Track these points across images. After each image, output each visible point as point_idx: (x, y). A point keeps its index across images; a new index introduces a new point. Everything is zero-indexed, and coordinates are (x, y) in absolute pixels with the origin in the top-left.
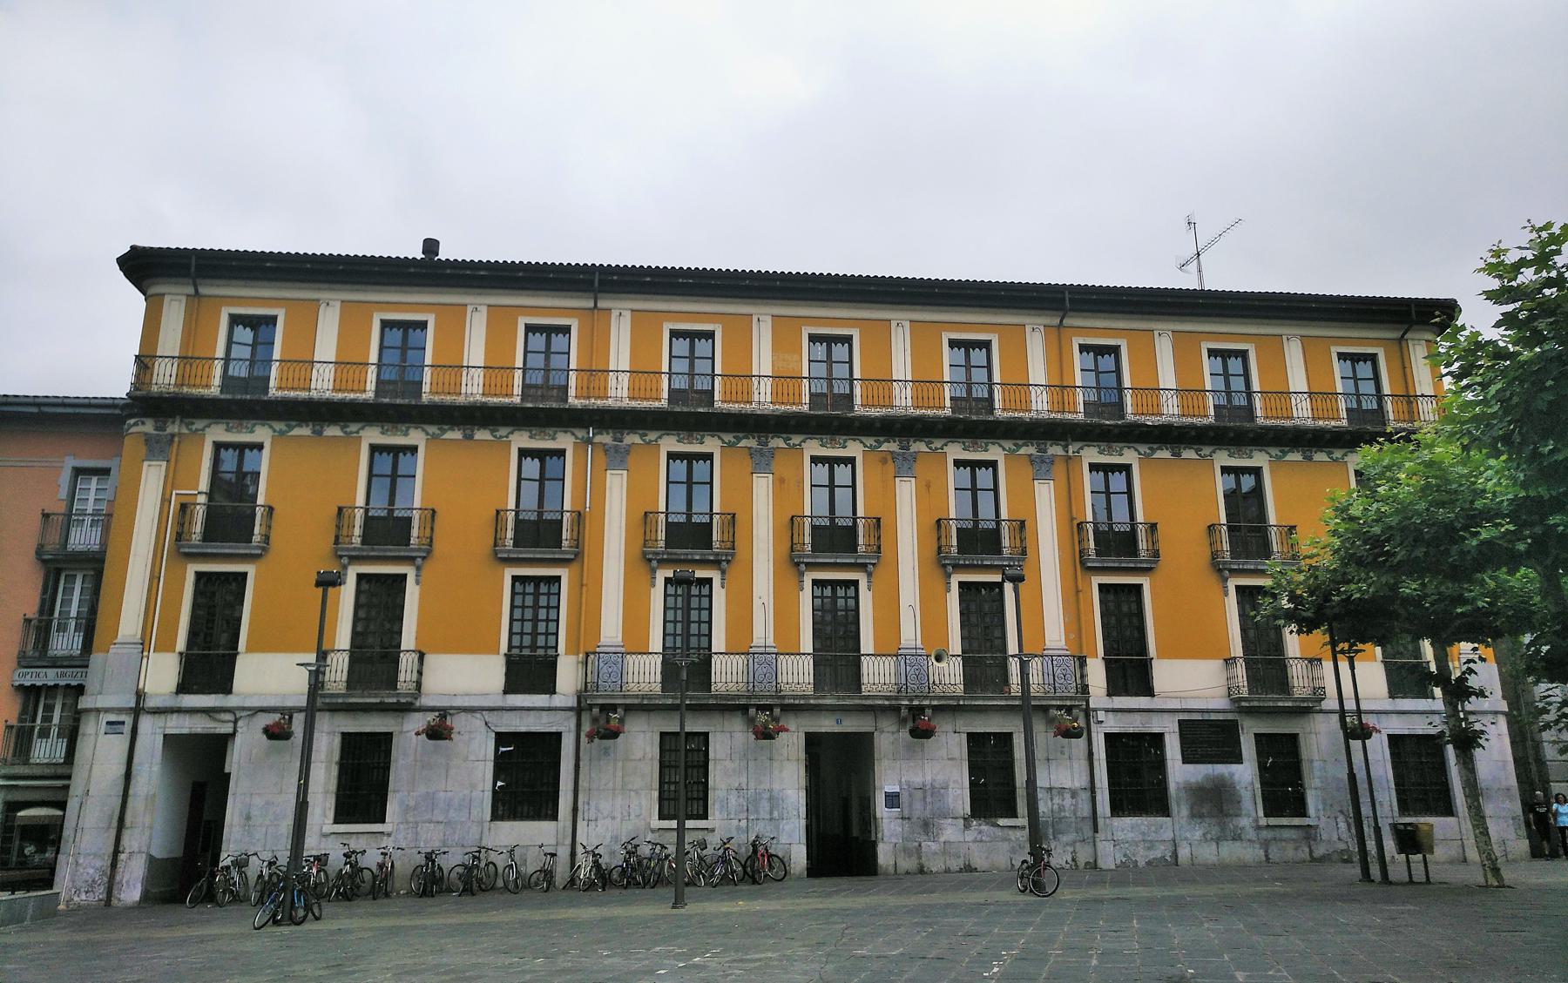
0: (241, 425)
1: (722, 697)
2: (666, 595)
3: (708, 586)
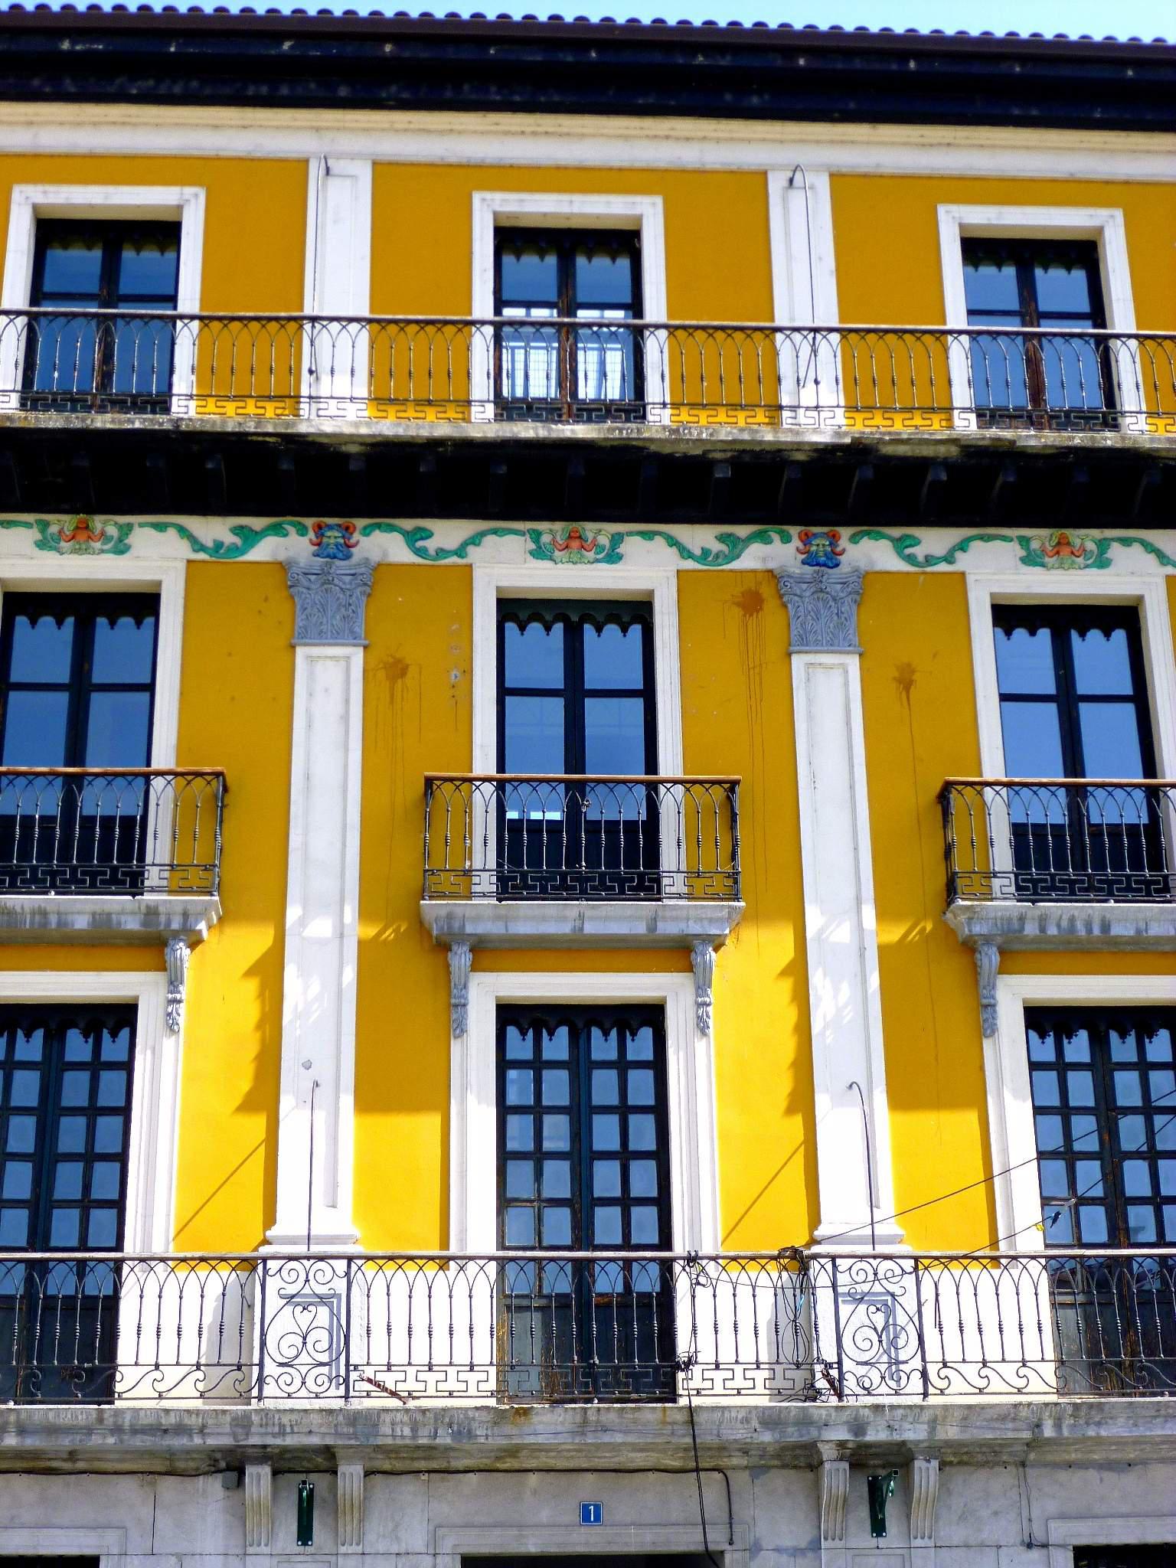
2: (503, 1065)
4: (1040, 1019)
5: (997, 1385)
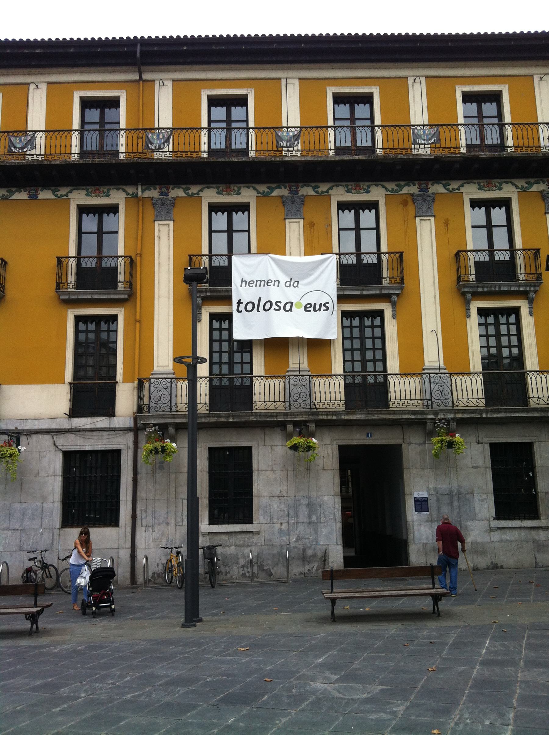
0: (230, 188)
1: (261, 415)
3: (227, 322)
4: (482, 312)
5: (461, 405)
